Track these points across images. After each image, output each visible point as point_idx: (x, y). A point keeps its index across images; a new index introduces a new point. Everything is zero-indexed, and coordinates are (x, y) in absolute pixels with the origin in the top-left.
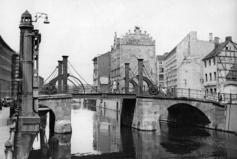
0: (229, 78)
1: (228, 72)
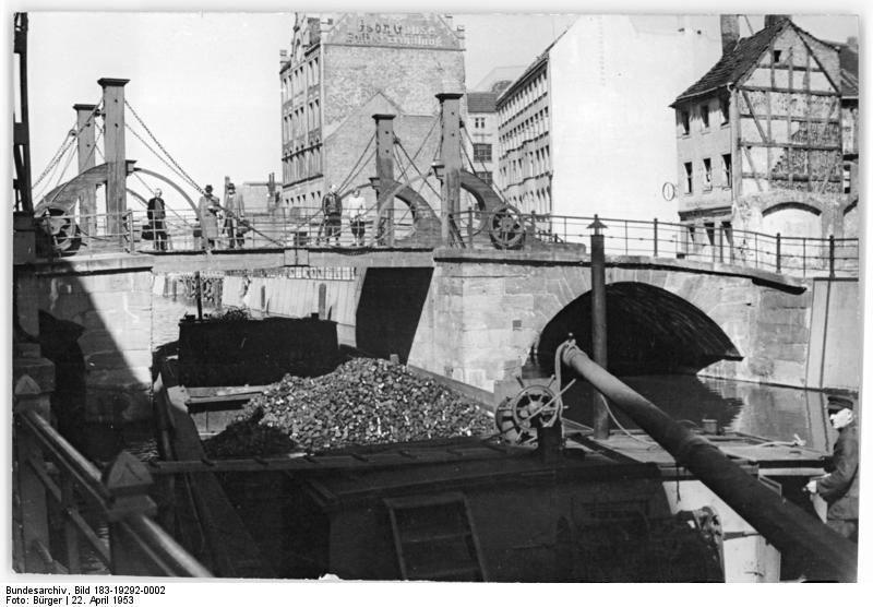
0: (782, 179)
1: (778, 153)
